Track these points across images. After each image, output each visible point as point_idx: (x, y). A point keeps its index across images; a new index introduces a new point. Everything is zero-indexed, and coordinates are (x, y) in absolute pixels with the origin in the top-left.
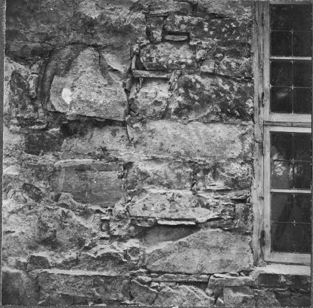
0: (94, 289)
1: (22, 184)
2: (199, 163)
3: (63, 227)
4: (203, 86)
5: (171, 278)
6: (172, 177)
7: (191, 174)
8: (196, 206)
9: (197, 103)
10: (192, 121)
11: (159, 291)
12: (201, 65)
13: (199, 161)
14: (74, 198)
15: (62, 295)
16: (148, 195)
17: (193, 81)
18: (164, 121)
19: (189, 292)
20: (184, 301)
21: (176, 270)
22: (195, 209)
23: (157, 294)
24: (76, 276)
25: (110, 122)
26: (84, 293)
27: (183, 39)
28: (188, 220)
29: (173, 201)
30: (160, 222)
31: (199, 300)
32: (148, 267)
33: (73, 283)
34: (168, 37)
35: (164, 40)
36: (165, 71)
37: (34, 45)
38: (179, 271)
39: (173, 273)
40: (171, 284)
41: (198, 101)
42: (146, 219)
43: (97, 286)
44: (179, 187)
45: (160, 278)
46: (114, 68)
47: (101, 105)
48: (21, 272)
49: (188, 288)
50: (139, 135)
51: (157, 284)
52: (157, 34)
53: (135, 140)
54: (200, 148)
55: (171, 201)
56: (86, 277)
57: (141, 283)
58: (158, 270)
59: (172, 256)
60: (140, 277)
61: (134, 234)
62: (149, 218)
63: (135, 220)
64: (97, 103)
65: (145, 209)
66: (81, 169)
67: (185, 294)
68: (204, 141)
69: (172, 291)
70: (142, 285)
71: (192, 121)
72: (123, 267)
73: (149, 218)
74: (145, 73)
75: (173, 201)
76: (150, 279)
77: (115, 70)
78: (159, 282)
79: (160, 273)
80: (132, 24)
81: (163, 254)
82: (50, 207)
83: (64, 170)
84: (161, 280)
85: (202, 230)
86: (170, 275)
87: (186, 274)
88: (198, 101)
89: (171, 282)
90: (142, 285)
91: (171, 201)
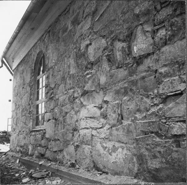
0: (150, 127)
1: (129, 89)
2: (179, 61)
3: (141, 103)
4: (177, 22)
5: (173, 120)
6: (171, 71)
7: (178, 68)
8: (181, 83)
9: (176, 32)
10: (176, 41)
11: (169, 126)
12: (176, 11)
13: (179, 60)
14: (144, 91)
15: (141, 130)
16: (163, 83)
17: (174, 21)
18: (167, 45)
19: (180, 125)
20: (178, 130)
21: (175, 116)
22: (181, 84)
23: (168, 128)
24: (143, 123)
25: (149, 54)
26: (147, 129)
27: (168, 3)
28: (178, 91)
29: (172, 83)
30: (168, 94)
31: (183, 129)
32: (166, 116)
33: (143, 125)
34: (163, 6)
35: (162, 8)
36: (163, 22)
37: (126, 34)
38: (176, 116)
39: (174, 117)
40: (174, 122)
41: (177, 30)
42: (164, 94)
43: (150, 126)
44: (175, 76)
45: (169, 121)
46: (147, 30)
47: (145, 48)
48: (132, 123)
49: (179, 123)
50: (158, 56)
51: (168, 123)
52: (159, 7)
53: (157, 59)
54: (179, 54)
55: (171, 83)
56: (146, 122)
57: (163, 123)
58: (169, 116)
59: (174, 109)
60: (162, 120)
61: (161, 102)
62: (165, 93)
63: (160, 95)
64: (143, 48)
65: (163, 89)
66: (143, 78)
67: (178, 127)
68: (180, 49)
69: (174, 125)
70: (162, 124)
71: (176, 41)
72: (157, 117)
73: (165, 93)
74: (157, 27)
75: (172, 83)
76: (165, 121)
77: (148, 31)
78: (169, 122)
79: (170, 118)
80: (149, 8)
81: (170, 109)
82: (138, 96)
83: (139, 80)
84: (170, 121)
85: (184, 94)
86: (173, 118)
87: (179, 117)
88: (177, 30)
89: (174, 121)
90: (162, 124)
91: (171, 83)
